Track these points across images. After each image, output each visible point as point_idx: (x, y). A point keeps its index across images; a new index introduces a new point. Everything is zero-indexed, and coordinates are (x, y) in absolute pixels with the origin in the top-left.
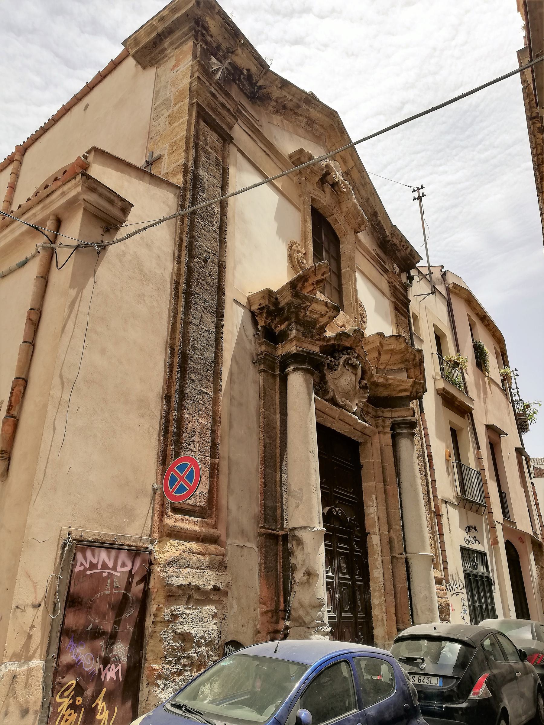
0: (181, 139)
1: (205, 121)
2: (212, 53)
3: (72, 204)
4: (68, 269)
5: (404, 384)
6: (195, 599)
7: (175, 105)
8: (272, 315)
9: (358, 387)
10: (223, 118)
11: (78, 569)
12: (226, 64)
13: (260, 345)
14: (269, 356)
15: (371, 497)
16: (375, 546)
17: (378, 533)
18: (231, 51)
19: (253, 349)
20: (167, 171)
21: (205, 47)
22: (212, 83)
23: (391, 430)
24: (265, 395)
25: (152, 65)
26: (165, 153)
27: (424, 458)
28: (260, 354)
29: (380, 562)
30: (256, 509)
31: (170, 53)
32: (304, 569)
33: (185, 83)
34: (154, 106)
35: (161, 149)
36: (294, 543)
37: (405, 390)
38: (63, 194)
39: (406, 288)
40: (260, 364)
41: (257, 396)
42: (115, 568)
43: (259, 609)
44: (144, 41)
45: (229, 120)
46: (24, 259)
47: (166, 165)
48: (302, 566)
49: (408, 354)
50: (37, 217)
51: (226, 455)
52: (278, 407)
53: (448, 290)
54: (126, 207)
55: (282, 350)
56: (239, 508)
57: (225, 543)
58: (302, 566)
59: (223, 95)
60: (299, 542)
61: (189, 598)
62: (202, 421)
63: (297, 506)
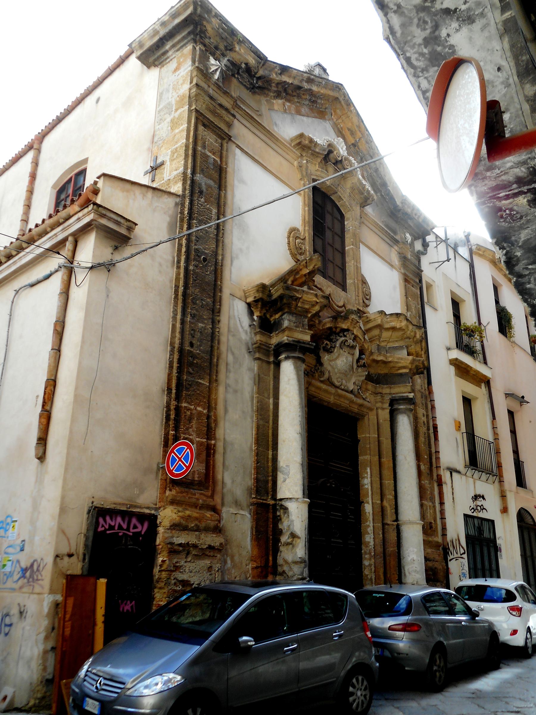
0: (181, 146)
1: (204, 125)
2: (210, 54)
3: (86, 229)
4: (85, 288)
5: (403, 362)
6: (194, 555)
7: (176, 110)
8: (270, 304)
9: (355, 366)
10: (220, 117)
11: (100, 529)
12: (225, 61)
13: (256, 334)
14: (263, 345)
15: (366, 469)
16: (367, 514)
17: (370, 502)
18: (229, 48)
19: (248, 339)
20: (169, 178)
21: (204, 49)
22: (210, 85)
23: (389, 406)
24: (259, 381)
25: (156, 66)
26: (167, 159)
27: (428, 429)
28: (255, 344)
29: (372, 528)
30: (250, 482)
31: (172, 55)
32: (289, 533)
33: (185, 88)
34: (158, 109)
35: (164, 156)
36: (282, 511)
37: (404, 367)
38: (79, 219)
39: (418, 256)
40: (255, 352)
41: (251, 382)
42: (128, 529)
43: (250, 565)
44: (148, 44)
45: (227, 119)
46: (48, 272)
47: (168, 172)
48: (288, 530)
49: (409, 332)
50: (58, 237)
51: (222, 437)
52: (271, 391)
53: (471, 252)
54: (131, 225)
55: (275, 340)
56: (233, 482)
57: (221, 511)
58: (288, 530)
59: (222, 95)
60: (286, 509)
61: (188, 554)
62: (199, 409)
63: (285, 481)
